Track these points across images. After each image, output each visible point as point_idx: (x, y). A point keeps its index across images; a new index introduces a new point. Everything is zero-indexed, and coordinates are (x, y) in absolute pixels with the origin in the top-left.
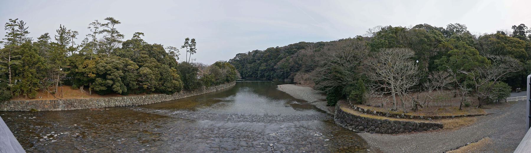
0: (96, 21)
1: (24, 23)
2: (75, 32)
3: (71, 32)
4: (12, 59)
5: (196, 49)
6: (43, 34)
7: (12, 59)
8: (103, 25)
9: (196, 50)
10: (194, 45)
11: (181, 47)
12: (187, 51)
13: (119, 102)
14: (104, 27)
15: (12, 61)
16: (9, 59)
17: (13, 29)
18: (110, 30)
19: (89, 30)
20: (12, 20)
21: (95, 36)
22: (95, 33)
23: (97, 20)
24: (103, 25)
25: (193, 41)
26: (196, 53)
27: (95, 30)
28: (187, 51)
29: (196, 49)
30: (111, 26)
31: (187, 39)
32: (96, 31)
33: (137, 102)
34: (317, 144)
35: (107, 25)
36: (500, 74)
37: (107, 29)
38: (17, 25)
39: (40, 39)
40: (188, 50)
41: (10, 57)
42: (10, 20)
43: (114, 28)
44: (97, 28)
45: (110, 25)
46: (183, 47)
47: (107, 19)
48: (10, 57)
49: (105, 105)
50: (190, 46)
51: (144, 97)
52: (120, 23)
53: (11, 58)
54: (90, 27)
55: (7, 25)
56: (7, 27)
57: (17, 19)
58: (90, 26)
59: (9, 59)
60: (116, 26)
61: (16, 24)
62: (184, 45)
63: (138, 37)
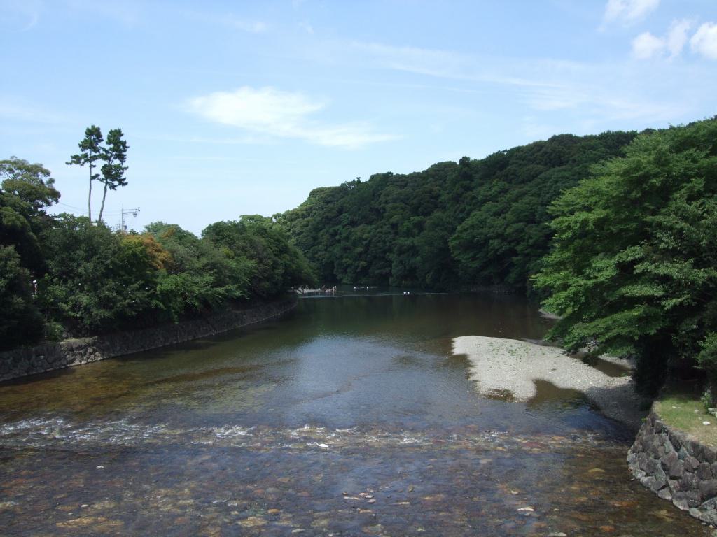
12: (93, 178)
25: (115, 136)
40: (93, 174)
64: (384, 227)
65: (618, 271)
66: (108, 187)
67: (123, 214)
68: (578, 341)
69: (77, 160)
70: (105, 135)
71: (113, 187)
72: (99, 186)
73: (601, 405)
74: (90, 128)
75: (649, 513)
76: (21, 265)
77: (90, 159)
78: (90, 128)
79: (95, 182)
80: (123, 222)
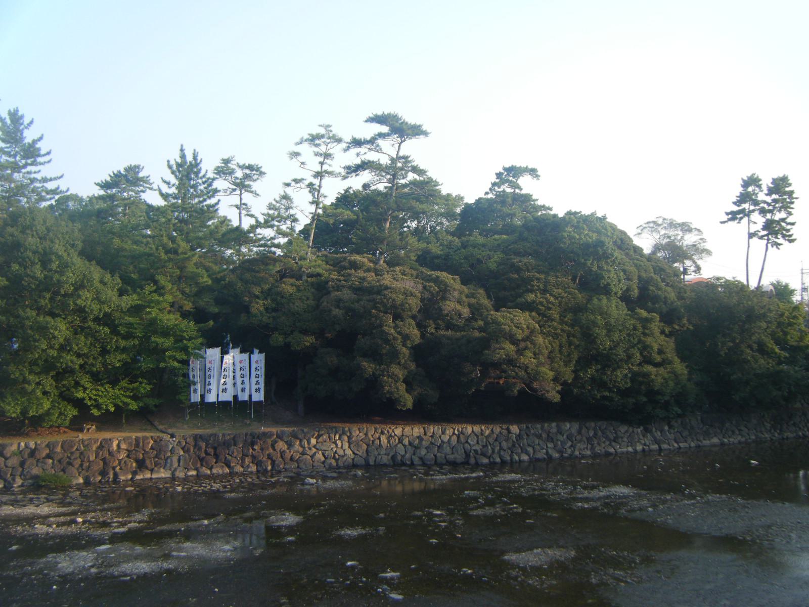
0: (322, 131)
1: (26, 121)
2: (250, 167)
3: (232, 166)
5: (49, 153)
6: (121, 167)
8: (357, 143)
9: (789, 227)
10: (786, 206)
11: (725, 218)
12: (751, 235)
14: (362, 150)
18: (385, 160)
19: (295, 162)
21: (320, 186)
22: (319, 175)
23: (329, 126)
24: (357, 143)
25: (780, 186)
26: (791, 241)
27: (322, 163)
28: (751, 235)
29: (49, 153)
30: (388, 149)
31: (752, 181)
32: (325, 167)
33: (485, 449)
35: (372, 141)
36: (104, 510)
37: (372, 156)
39: (105, 186)
40: (752, 231)
43: (401, 154)
44: (327, 156)
46: (733, 216)
49: (353, 456)
50: (763, 212)
51: (515, 429)
52: (426, 134)
54: (297, 154)
58: (297, 149)
60: (412, 148)
62: (736, 208)
63: (516, 186)
64: (399, 237)
65: (575, 394)
66: (769, 245)
67: (802, 273)
68: (86, 344)
69: (733, 216)
70: (766, 182)
71: (777, 245)
72: (758, 245)
73: (726, 533)
74: (20, 114)
75: (446, 524)
76: (416, 261)
77: (747, 214)
78: (20, 114)
79: (755, 240)
80: (803, 284)
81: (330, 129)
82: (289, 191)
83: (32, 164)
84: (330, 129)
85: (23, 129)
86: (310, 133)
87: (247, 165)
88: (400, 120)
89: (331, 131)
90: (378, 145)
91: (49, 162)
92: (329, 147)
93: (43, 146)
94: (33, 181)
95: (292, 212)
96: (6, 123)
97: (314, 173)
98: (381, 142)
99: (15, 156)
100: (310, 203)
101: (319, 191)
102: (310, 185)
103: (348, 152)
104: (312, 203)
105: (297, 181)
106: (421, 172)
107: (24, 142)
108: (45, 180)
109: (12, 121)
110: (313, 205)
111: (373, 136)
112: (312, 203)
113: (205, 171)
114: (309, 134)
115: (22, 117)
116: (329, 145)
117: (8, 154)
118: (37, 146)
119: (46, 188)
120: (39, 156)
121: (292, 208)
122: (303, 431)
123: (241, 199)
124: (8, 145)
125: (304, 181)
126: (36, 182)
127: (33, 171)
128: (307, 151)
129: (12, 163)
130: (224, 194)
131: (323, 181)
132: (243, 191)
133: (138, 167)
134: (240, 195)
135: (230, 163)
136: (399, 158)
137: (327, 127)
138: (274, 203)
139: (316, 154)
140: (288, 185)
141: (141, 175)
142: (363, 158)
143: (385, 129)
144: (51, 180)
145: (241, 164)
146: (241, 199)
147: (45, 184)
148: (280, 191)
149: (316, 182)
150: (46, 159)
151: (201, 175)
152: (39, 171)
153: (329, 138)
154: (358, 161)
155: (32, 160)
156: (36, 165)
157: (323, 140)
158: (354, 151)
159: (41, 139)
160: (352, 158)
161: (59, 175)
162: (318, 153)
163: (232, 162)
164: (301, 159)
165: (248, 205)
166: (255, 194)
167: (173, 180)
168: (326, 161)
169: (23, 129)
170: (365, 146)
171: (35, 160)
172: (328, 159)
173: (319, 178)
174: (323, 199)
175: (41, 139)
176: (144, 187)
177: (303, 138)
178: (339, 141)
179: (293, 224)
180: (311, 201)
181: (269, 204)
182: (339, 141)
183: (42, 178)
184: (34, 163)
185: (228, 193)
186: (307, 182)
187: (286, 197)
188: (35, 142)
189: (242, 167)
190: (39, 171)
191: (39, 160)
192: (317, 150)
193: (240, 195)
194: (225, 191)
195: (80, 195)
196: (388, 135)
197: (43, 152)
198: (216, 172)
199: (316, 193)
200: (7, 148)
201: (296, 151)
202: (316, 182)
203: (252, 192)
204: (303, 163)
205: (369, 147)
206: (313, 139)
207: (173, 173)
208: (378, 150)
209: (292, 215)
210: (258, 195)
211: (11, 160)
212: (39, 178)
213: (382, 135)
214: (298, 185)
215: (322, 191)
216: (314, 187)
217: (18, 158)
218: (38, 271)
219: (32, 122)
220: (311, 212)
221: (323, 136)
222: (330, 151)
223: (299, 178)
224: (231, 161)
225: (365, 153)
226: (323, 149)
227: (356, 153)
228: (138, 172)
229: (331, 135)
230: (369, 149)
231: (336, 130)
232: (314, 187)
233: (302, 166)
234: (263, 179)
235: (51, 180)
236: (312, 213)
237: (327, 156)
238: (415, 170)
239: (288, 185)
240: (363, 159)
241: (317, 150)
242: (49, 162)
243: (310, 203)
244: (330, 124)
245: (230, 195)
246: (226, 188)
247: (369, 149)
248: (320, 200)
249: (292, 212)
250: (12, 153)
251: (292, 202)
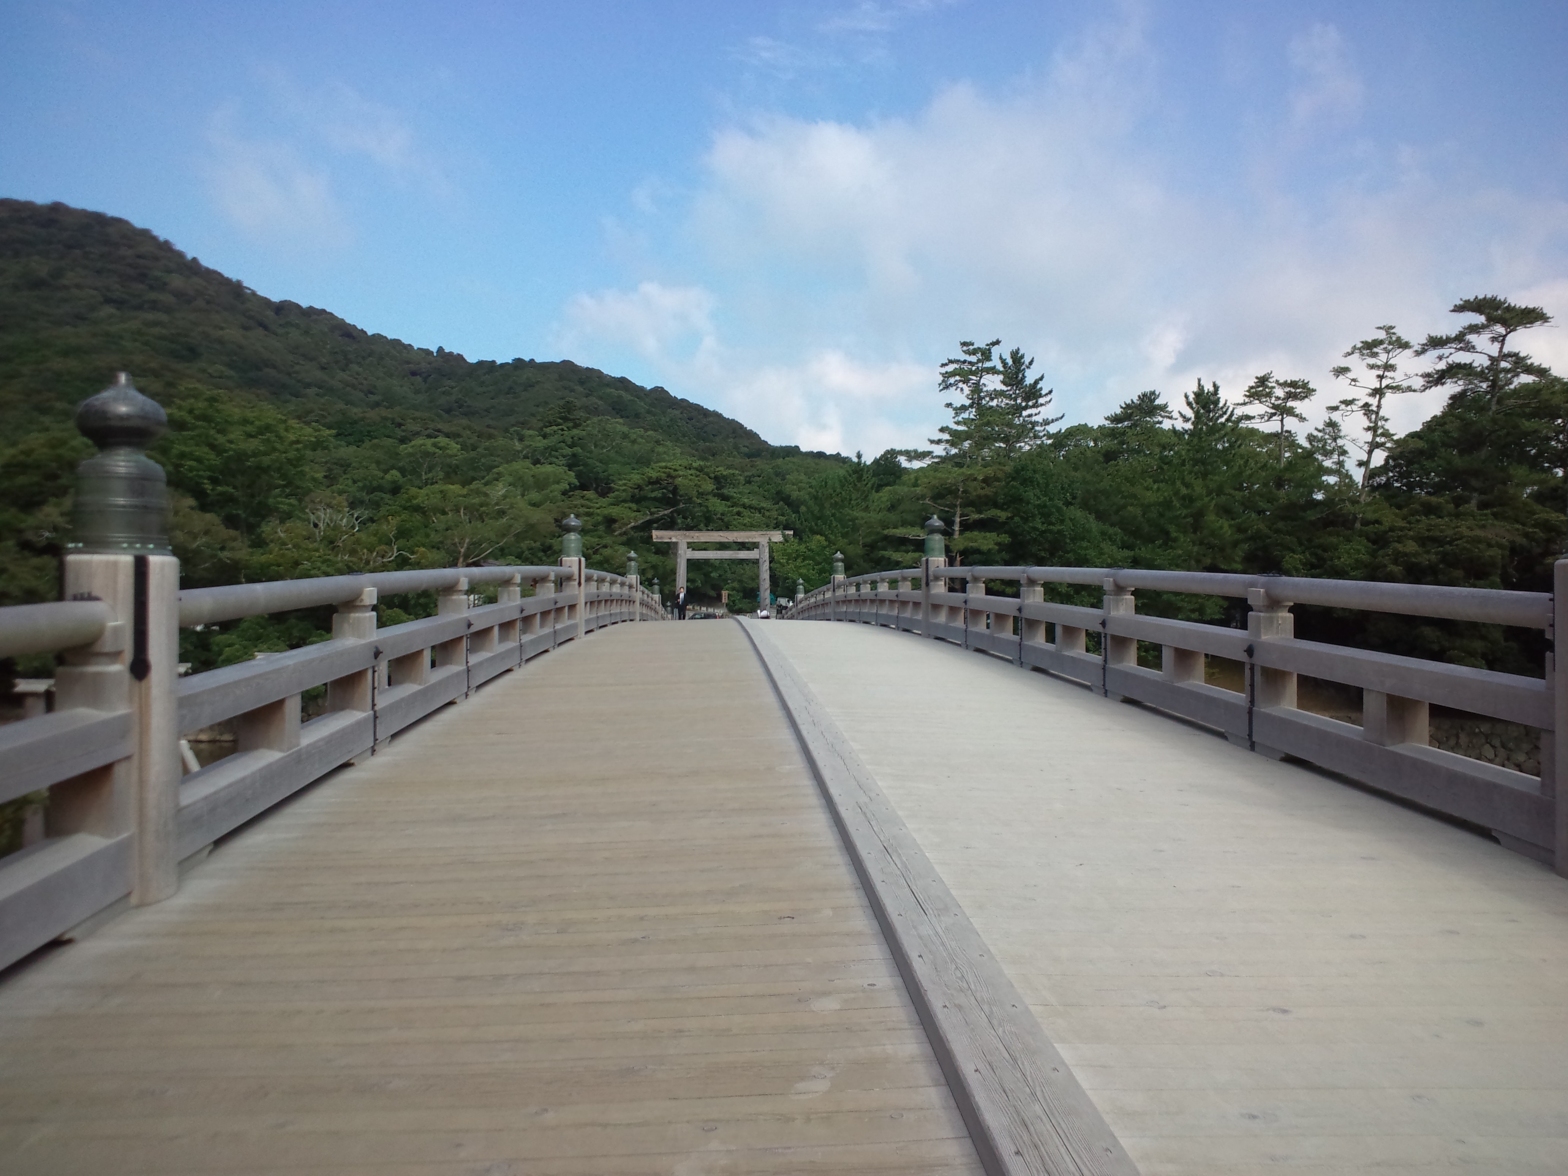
0: (1382, 335)
1: (1027, 360)
2: (1293, 384)
4: (966, 527)
7: (966, 527)
13: (1503, 746)
14: (1445, 351)
15: (968, 534)
16: (957, 528)
17: (977, 389)
18: (1480, 361)
20: (972, 344)
22: (1378, 392)
23: (1392, 328)
24: (1435, 343)
27: (1381, 377)
29: (1050, 392)
34: (536, 462)
35: (1460, 338)
37: (1463, 358)
38: (998, 372)
41: (958, 520)
42: (964, 344)
45: (1482, 342)
47: (1459, 309)
48: (958, 520)
53: (961, 522)
55: (951, 368)
56: (952, 380)
57: (997, 342)
58: (1343, 363)
59: (957, 528)
61: (988, 364)
74: (1021, 352)
81: (1392, 331)
82: (1336, 416)
83: (1033, 406)
84: (1392, 331)
85: (1024, 369)
86: (1364, 340)
87: (1289, 381)
88: (1505, 304)
89: (1394, 334)
90: (1469, 342)
91: (1050, 401)
92: (1390, 356)
93: (1044, 387)
94: (1035, 424)
95: (1340, 442)
96: (1007, 364)
97: (1371, 391)
98: (1472, 338)
99: (1015, 399)
100: (1364, 429)
101: (1377, 413)
102: (1366, 405)
103: (1422, 356)
104: (1369, 429)
105: (1347, 403)
106: (1541, 372)
107: (1025, 383)
108: (1046, 422)
109: (1014, 362)
110: (1369, 432)
111: (1461, 329)
112: (1369, 429)
113: (1224, 402)
114: (1362, 342)
115: (1022, 357)
116: (1391, 354)
117: (1009, 397)
118: (1039, 386)
119: (1047, 431)
120: (1041, 396)
121: (1340, 437)
122: (1350, 718)
123: (1282, 425)
124: (1009, 388)
125: (1356, 402)
126: (1037, 425)
127: (1034, 413)
128: (1358, 365)
129: (1013, 405)
130: (1259, 421)
131: (1383, 401)
132: (1285, 416)
133: (1153, 393)
134: (1282, 421)
135: (1267, 380)
136: (1504, 356)
137: (1389, 329)
138: (1315, 433)
139: (1372, 367)
140: (1335, 409)
141: (1158, 402)
142: (1450, 361)
143: (1480, 319)
144: (1053, 421)
145: (1281, 381)
146: (1282, 425)
147: (1047, 428)
148: (1325, 416)
149: (1374, 401)
150: (1048, 398)
151: (1221, 405)
152: (1039, 413)
153: (1390, 343)
154: (1442, 365)
155: (1034, 401)
156: (1037, 407)
157: (1382, 347)
158: (1433, 353)
159: (1041, 378)
160: (1431, 362)
161: (1061, 415)
162: (1373, 365)
163: (1271, 380)
164: (1351, 375)
165: (1292, 432)
166: (1301, 418)
167: (1190, 414)
168: (1386, 373)
169: (1024, 369)
170: (1449, 345)
171: (1037, 402)
172: (1389, 371)
173: (1378, 396)
174: (1383, 422)
175: (1041, 378)
176: (1162, 417)
177: (1355, 346)
178: (1405, 346)
179: (1341, 458)
180: (1366, 427)
181: (1308, 435)
182: (1405, 346)
183: (1044, 420)
184: (1035, 406)
185: (1266, 418)
186: (1361, 403)
187: (1332, 424)
188: (1036, 382)
189: (1285, 384)
190: (1039, 413)
191: (1041, 401)
192: (1372, 361)
193: (1282, 421)
194: (1262, 417)
195: (1090, 426)
196: (1484, 327)
197: (1043, 392)
198: (1248, 394)
199: (1373, 417)
200: (1008, 391)
201: (1342, 366)
202: (1374, 401)
203: (1297, 416)
204: (1354, 380)
205: (1455, 346)
206: (1369, 347)
207: (1189, 404)
208: (1469, 348)
209: (1340, 447)
210: (1305, 419)
211: (1012, 402)
212: (1041, 421)
213: (1474, 329)
214: (1349, 408)
215: (1381, 413)
216: (1370, 408)
217: (1019, 401)
218: (1038, 523)
219: (1031, 363)
220: (1367, 441)
221: (1381, 342)
222: (1391, 362)
223: (1350, 398)
224: (1268, 378)
225: (1451, 354)
226: (1383, 358)
227: (1437, 355)
228: (1155, 399)
229: (1394, 339)
230: (1456, 348)
231: (1401, 332)
232: (1370, 408)
233: (1353, 383)
234: (1312, 398)
235: (1053, 421)
236: (1368, 443)
237: (1389, 367)
238: (1530, 370)
239: (1335, 409)
240: (1451, 362)
241: (1372, 361)
242: (1050, 401)
243: (1364, 429)
244: (1393, 325)
245: (1268, 420)
246: (1263, 413)
247: (1456, 348)
248: (1380, 424)
249: (1340, 442)
250: (1013, 396)
251: (1339, 431)
